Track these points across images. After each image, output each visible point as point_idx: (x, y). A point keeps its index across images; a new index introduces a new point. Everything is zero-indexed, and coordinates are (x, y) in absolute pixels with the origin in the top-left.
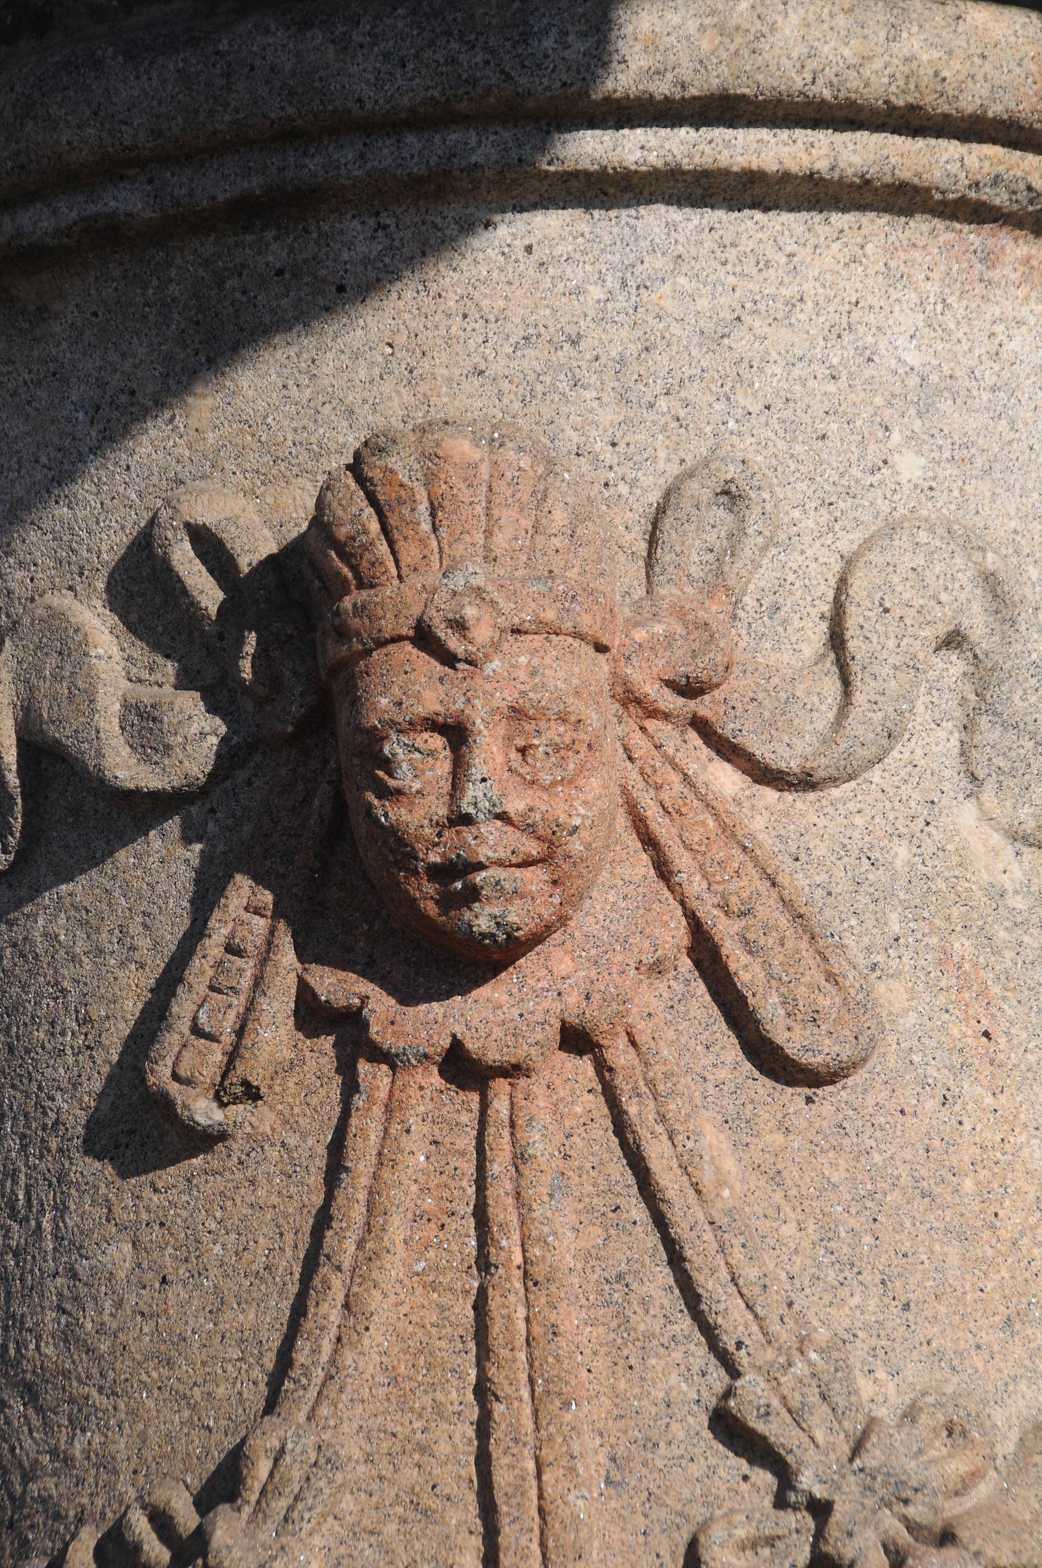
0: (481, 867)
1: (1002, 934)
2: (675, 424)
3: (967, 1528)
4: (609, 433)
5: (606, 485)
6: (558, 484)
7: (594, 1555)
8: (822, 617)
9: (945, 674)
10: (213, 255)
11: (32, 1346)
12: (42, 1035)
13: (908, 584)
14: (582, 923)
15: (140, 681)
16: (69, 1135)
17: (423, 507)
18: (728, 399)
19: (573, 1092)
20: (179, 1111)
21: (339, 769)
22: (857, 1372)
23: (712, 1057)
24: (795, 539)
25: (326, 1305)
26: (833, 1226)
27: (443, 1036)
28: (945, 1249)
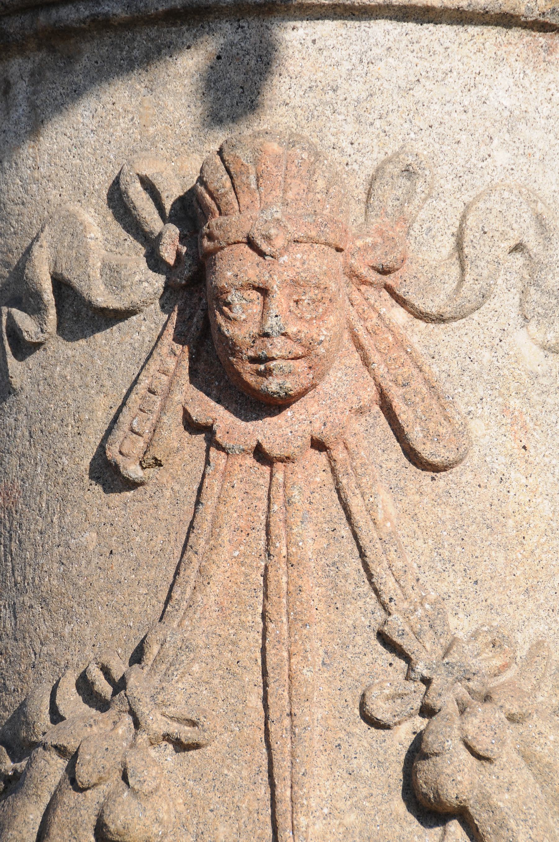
0: (273, 359)
1: (536, 398)
2: (384, 134)
3: (497, 694)
4: (350, 138)
5: (347, 164)
6: (321, 166)
7: (315, 699)
8: (453, 235)
9: (514, 264)
10: (156, 36)
11: (46, 580)
12: (57, 426)
13: (497, 219)
14: (324, 387)
15: (111, 251)
16: (68, 477)
17: (253, 177)
18: (411, 122)
19: (315, 471)
20: (121, 470)
21: (207, 304)
22: (449, 614)
23: (385, 456)
24: (441, 195)
25: (189, 571)
26: (441, 542)
27: (252, 441)
28: (497, 554)
